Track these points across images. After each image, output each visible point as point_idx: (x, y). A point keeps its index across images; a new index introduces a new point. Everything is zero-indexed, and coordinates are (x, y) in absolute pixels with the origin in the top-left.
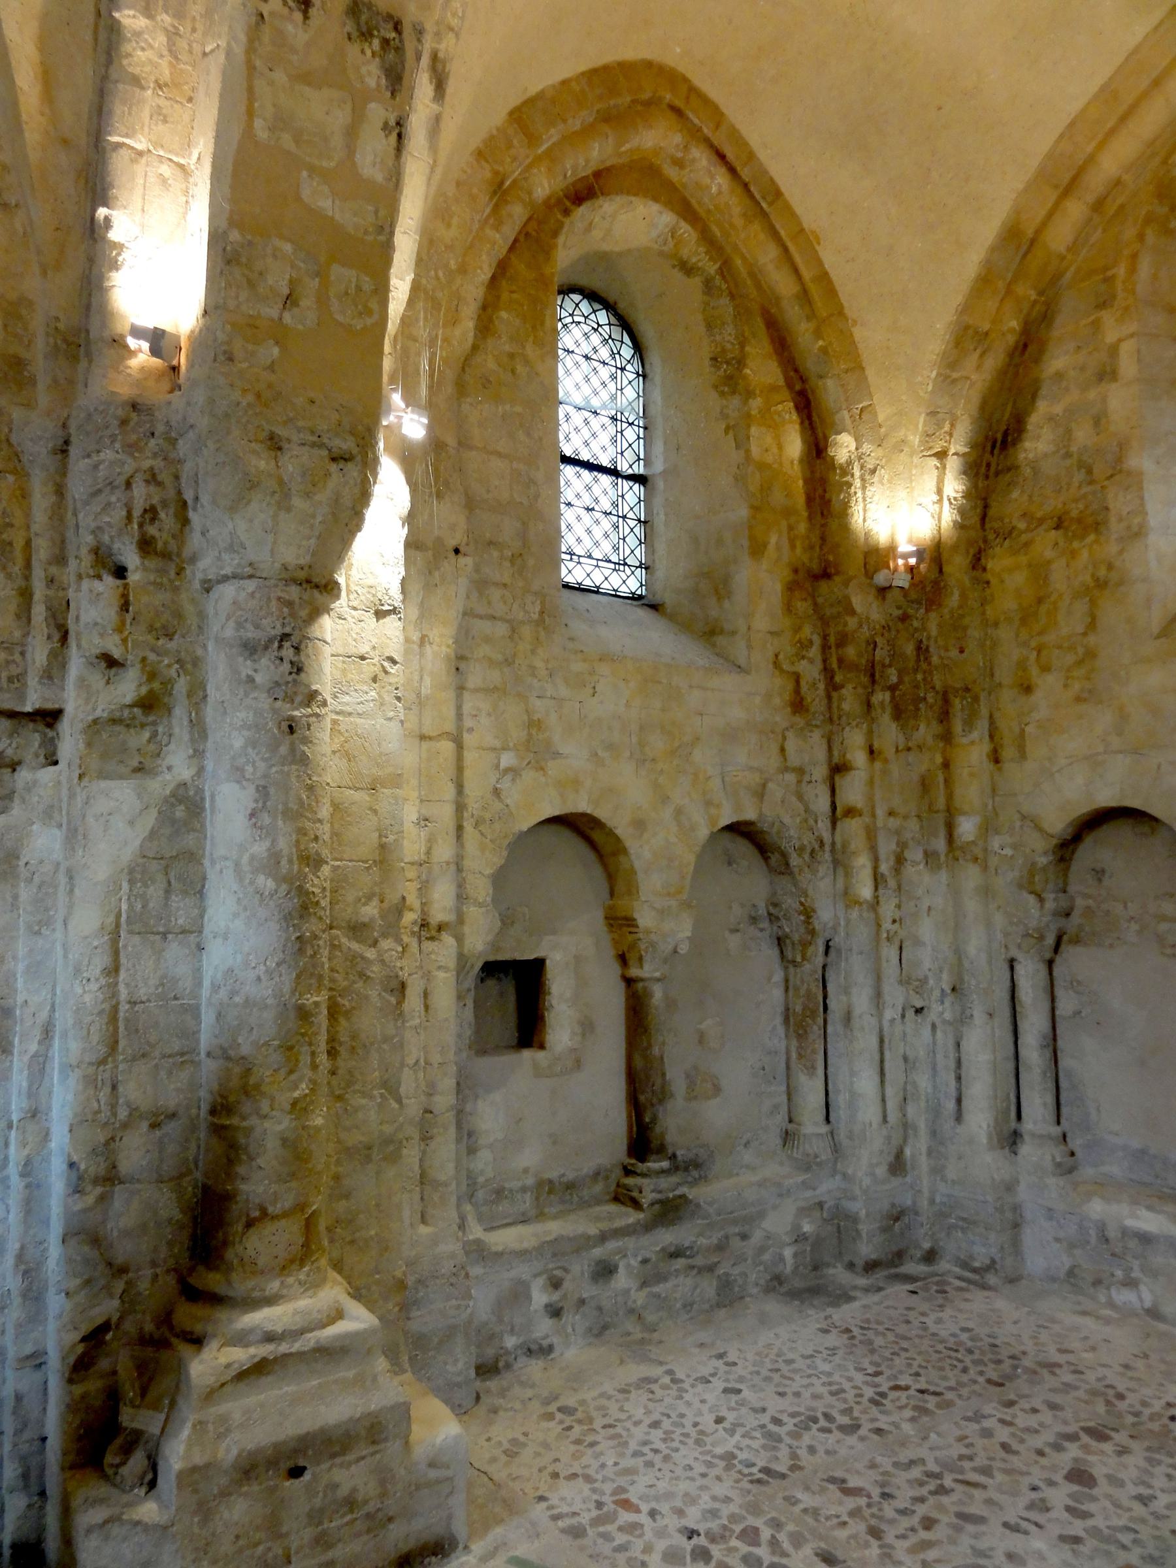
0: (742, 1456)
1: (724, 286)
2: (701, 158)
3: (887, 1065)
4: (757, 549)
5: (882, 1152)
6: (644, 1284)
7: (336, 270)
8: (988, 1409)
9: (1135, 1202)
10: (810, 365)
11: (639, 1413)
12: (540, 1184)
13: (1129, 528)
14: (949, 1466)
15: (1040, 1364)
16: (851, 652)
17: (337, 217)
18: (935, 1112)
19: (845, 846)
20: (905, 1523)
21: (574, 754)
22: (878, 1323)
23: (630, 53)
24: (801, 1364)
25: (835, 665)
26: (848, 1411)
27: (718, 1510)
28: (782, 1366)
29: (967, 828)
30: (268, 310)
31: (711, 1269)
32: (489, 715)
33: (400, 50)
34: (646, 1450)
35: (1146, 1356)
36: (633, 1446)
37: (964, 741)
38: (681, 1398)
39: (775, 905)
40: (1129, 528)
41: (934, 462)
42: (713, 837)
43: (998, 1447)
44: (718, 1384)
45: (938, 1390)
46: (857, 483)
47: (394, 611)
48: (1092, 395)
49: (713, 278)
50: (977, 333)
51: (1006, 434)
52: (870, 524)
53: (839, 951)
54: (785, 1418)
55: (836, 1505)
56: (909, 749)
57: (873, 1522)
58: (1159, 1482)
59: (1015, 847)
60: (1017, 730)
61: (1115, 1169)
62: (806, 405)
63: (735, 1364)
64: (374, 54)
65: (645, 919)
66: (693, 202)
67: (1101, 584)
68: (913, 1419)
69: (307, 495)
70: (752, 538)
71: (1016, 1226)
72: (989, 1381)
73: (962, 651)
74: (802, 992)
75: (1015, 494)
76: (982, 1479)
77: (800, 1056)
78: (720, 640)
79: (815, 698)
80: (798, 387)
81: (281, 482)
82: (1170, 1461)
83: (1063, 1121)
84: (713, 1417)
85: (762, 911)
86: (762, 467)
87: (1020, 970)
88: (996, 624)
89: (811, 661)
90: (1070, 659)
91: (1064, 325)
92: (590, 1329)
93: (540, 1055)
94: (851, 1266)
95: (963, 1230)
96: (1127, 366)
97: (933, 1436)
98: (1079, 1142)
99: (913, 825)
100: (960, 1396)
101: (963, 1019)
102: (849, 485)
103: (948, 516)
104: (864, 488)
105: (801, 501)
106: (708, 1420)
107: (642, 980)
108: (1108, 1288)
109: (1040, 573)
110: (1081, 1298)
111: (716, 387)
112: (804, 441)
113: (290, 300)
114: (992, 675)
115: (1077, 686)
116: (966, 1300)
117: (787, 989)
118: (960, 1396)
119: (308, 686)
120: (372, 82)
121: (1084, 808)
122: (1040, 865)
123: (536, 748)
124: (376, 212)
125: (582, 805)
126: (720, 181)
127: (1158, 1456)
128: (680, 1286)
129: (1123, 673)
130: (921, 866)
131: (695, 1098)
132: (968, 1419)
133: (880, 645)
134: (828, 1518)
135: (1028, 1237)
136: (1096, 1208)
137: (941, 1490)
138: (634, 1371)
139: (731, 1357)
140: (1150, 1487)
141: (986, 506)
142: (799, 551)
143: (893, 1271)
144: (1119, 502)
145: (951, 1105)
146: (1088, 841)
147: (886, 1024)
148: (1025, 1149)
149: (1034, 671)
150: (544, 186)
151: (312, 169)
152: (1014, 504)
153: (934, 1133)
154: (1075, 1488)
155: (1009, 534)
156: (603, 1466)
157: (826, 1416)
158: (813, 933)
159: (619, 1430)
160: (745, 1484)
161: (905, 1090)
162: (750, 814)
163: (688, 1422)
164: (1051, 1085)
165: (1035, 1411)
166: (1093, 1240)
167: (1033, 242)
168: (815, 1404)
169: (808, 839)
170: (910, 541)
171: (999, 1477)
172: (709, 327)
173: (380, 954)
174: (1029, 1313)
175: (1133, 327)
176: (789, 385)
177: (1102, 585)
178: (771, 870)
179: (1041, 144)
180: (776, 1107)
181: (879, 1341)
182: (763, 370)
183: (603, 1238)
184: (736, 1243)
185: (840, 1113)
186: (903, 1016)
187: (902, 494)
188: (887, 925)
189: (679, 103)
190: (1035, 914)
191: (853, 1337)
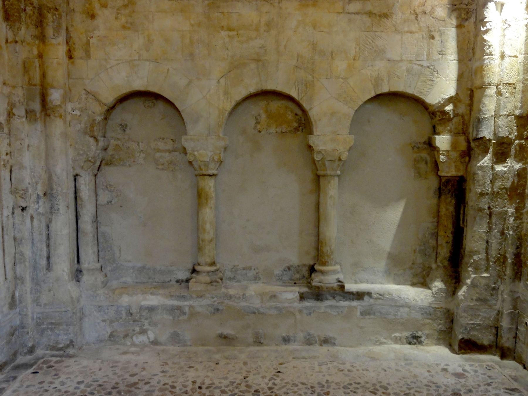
3: (6, 244)
5: (5, 297)
9: (144, 293)
35: (167, 364)
37: (54, 41)
56: (16, 42)
59: (81, 110)
60: (84, 40)
61: (129, 280)
71: (81, 319)
83: (100, 260)
87: (81, 181)
95: (52, 330)
98: (109, 269)
101: (52, 210)
108: (132, 338)
110: (117, 346)
115: (123, 20)
122: (97, 121)
129: (151, 17)
130: (24, 119)
135: (87, 323)
136: (125, 300)
143: (12, 365)
145: (44, 262)
147: (5, 219)
148: (85, 278)
161: (15, 258)
166: (124, 316)
174: (102, 362)
186: (13, 213)
190: (93, 149)
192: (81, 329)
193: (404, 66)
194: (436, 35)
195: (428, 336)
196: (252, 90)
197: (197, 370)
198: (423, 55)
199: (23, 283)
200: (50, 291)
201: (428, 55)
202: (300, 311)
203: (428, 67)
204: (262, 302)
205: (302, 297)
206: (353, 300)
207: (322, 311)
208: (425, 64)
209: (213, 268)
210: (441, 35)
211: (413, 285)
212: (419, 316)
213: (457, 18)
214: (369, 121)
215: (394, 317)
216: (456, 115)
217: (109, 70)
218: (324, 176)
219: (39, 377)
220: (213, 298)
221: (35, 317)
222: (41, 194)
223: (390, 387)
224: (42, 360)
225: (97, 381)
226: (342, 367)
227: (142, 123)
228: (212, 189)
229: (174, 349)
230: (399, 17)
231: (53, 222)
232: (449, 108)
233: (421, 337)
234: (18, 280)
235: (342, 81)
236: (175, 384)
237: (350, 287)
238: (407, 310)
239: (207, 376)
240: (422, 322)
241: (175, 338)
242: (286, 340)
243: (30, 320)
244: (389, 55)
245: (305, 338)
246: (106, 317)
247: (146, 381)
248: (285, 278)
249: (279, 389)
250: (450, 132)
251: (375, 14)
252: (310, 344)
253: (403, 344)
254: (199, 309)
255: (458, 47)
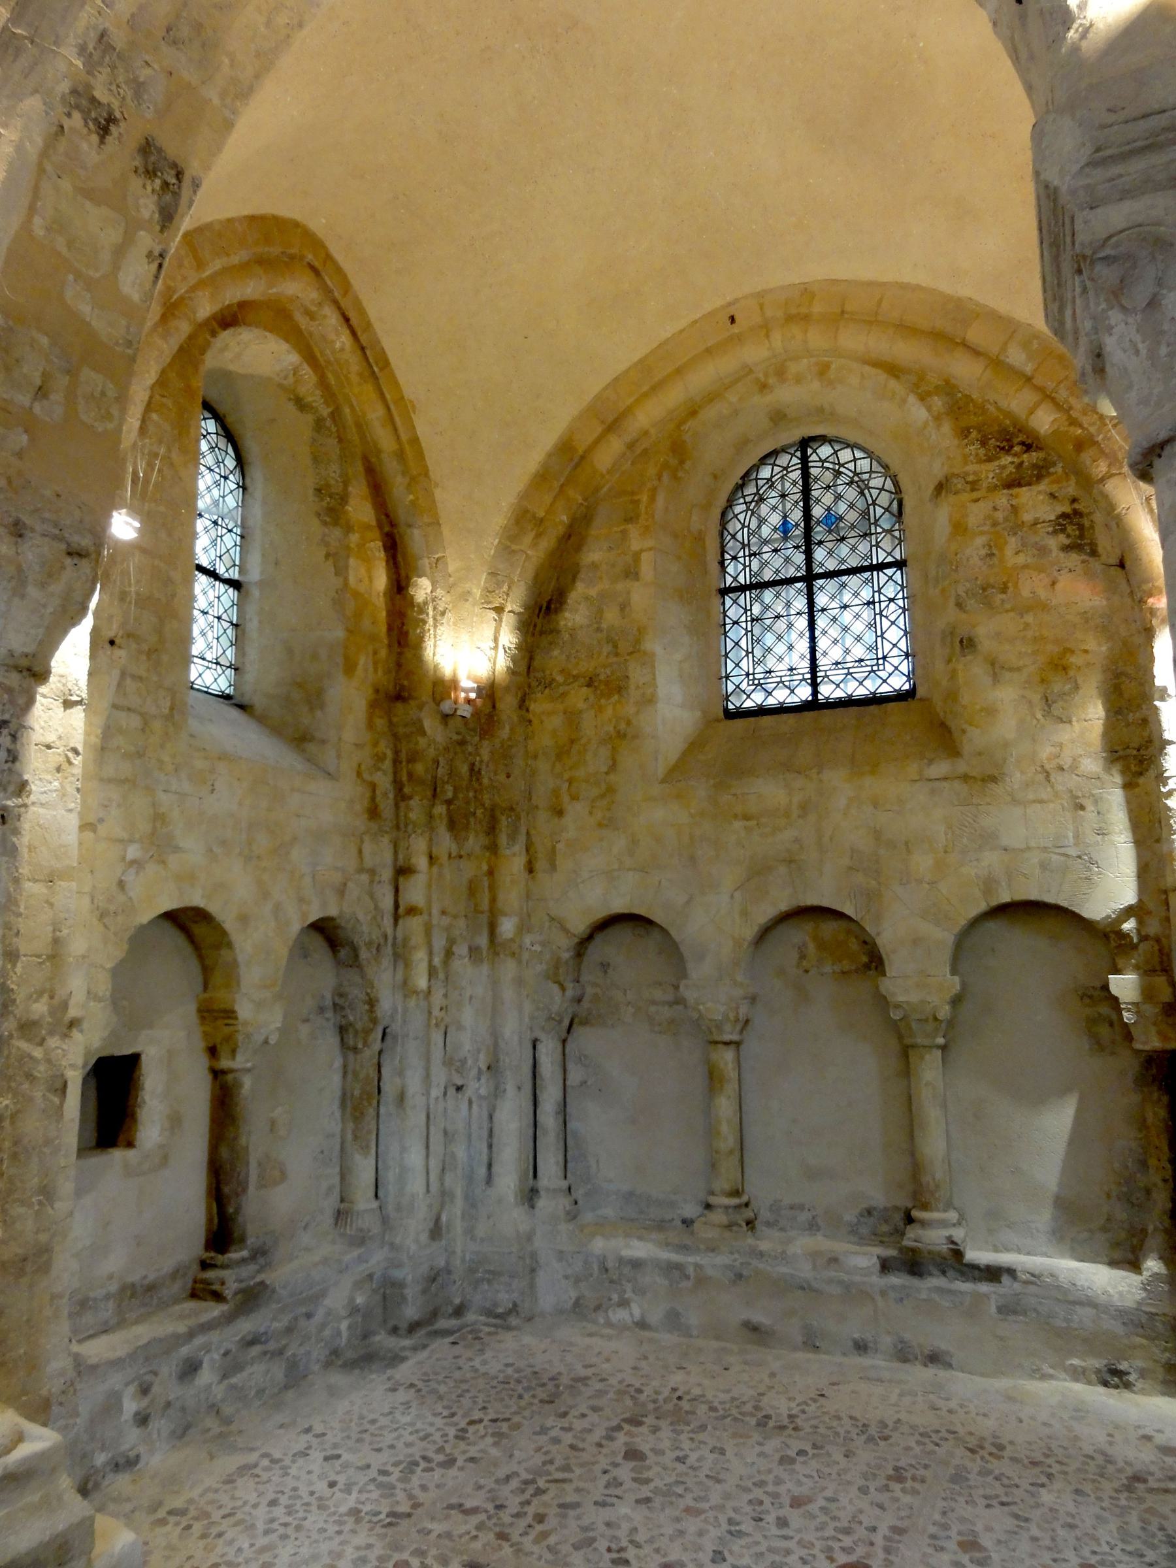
0: (367, 1508)
1: (334, 429)
2: (332, 319)
4: (349, 668)
5: (425, 1219)
6: (225, 1376)
7: (87, 374)
8: (549, 1422)
9: (627, 1235)
10: (401, 515)
11: (252, 1497)
12: (123, 1288)
13: (643, 695)
14: (538, 1473)
15: (573, 1380)
16: (419, 768)
17: (94, 323)
18: (470, 1178)
19: (406, 940)
20: (522, 1523)
21: (192, 848)
22: (436, 1374)
23: (284, 212)
24: (383, 1421)
25: (405, 779)
26: (440, 1450)
27: (366, 1556)
28: (368, 1426)
29: (507, 927)
30: (21, 397)
31: (280, 1352)
32: (119, 806)
33: (176, 195)
34: (275, 1525)
35: (646, 1358)
36: (261, 1526)
37: (508, 852)
38: (287, 1474)
39: (341, 995)
40: (643, 695)
41: (494, 614)
42: (302, 930)
43: (568, 1449)
44: (317, 1455)
45: (507, 1416)
46: (431, 621)
47: (80, 703)
48: (619, 587)
49: (324, 420)
50: (534, 517)
51: (549, 602)
52: (438, 659)
53: (395, 1038)
54: (390, 1468)
55: (463, 1525)
56: (461, 857)
57: (498, 1529)
58: (687, 1445)
59: (543, 944)
61: (609, 1212)
62: (393, 547)
63: (324, 1434)
64: (153, 190)
65: (244, 1011)
66: (316, 350)
67: (621, 735)
68: (495, 1444)
69: (43, 585)
70: (347, 658)
71: (533, 1270)
72: (541, 1401)
73: (508, 776)
74: (362, 1076)
75: (556, 653)
76: (566, 1475)
77: (356, 1138)
78: (311, 747)
79: (386, 806)
80: (387, 529)
81: (20, 569)
82: (689, 1428)
83: (569, 1175)
84: (324, 1485)
85: (328, 1002)
86: (356, 594)
88: (535, 757)
89: (385, 773)
90: (595, 792)
91: (597, 530)
92: (174, 1432)
93: (131, 1154)
94: (395, 1330)
95: (489, 1282)
96: (646, 568)
97: (516, 1453)
98: (581, 1191)
99: (462, 923)
100: (524, 1418)
101: (497, 1092)
102: (425, 622)
103: (502, 663)
104: (435, 627)
105: (383, 629)
106: (321, 1487)
107: (232, 1071)
108: (606, 1311)
109: (572, 719)
110: (584, 1324)
111: (318, 515)
112: (389, 577)
113: (41, 392)
114: (530, 799)
116: (499, 1342)
117: (345, 1073)
118: (524, 1418)
119: (20, 775)
120: (146, 214)
121: (601, 914)
123: (159, 841)
124: (128, 328)
125: (196, 899)
126: (343, 340)
127: (678, 1428)
128: (256, 1373)
131: (265, 1186)
132: (539, 1433)
133: (441, 764)
134: (460, 1537)
135: (542, 1278)
136: (599, 1245)
137: (539, 1492)
138: (230, 1463)
139: (318, 1428)
140: (682, 1450)
141: (531, 659)
142: (380, 673)
143: (430, 1328)
144: (637, 674)
145: (482, 1171)
146: (599, 938)
147: (432, 1101)
148: (542, 1203)
149: (566, 798)
150: (205, 308)
151: (78, 275)
152: (555, 660)
153: (466, 1197)
154: (632, 1464)
155: (549, 684)
156: (240, 1550)
157: (424, 1458)
158: (374, 1021)
159: (239, 1516)
160: (379, 1530)
161: (444, 1161)
162: (332, 912)
163: (303, 1492)
164: (562, 1143)
165: (584, 1416)
167: (583, 458)
168: (410, 1451)
169: (376, 935)
170: (469, 678)
171: (578, 1471)
172: (316, 460)
173: (46, 1053)
175: (650, 543)
176: (380, 526)
177: (622, 736)
178: (339, 963)
179: (595, 386)
180: (330, 1189)
181: (442, 1389)
182: (361, 510)
183: (191, 1335)
184: (303, 1323)
185: (390, 1189)
186: (445, 1094)
187: (465, 636)
188: (436, 1012)
189: (316, 264)
190: (557, 1001)
191: (419, 1391)
192: (532, 1286)
193: (1035, 858)
194: (1088, 803)
195: (1143, 1374)
196: (784, 907)
197: (689, 1373)
198: (1066, 837)
199: (452, 1202)
200: (489, 1218)
201: (1076, 836)
202: (883, 1293)
203: (1079, 857)
204: (814, 1268)
205: (886, 1266)
206: (980, 1280)
207: (924, 1296)
208: (1073, 852)
209: (735, 1201)
210: (1096, 802)
211: (1113, 1264)
212: (1120, 1330)
213: (1123, 773)
214: (993, 950)
215: (1064, 1325)
216: (1144, 938)
217: (581, 886)
218: (913, 1046)
219: (457, 1350)
220: (732, 1253)
221: (467, 1258)
222: (484, 1068)
223: (1009, 1448)
224: (469, 1329)
225: (532, 1366)
226: (940, 1403)
227: (627, 963)
228: (730, 1066)
229: (668, 1338)
230: (1016, 779)
231: (497, 1111)
232: (1129, 926)
233: (1128, 1373)
234: (445, 1195)
235: (927, 886)
236: (644, 1388)
237: (976, 1255)
238: (1089, 1311)
239: (699, 1385)
240: (1126, 1341)
241: (673, 1320)
242: (861, 1347)
243: (458, 1262)
244: (1005, 841)
245: (895, 1347)
246: (569, 1271)
247: (604, 1376)
248: (864, 1231)
249: (808, 1420)
250: (1137, 968)
251: (974, 778)
252: (905, 1360)
253: (1089, 1383)
254: (710, 1272)
255: (1130, 820)
